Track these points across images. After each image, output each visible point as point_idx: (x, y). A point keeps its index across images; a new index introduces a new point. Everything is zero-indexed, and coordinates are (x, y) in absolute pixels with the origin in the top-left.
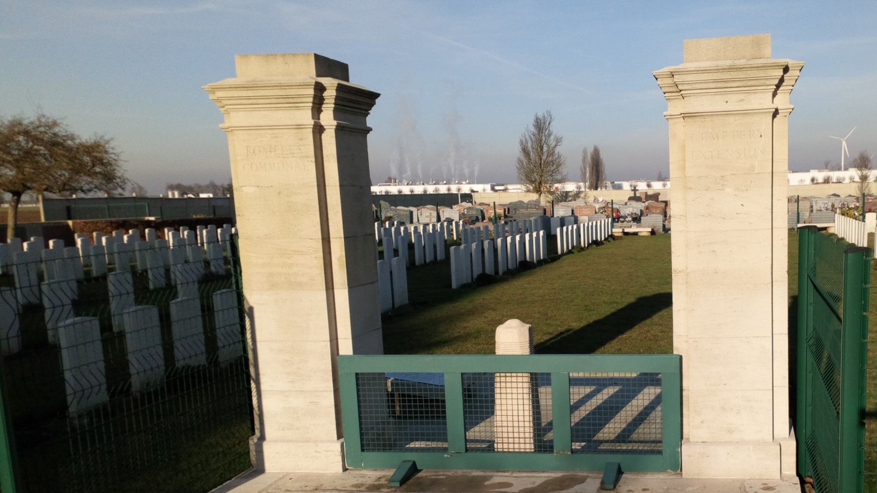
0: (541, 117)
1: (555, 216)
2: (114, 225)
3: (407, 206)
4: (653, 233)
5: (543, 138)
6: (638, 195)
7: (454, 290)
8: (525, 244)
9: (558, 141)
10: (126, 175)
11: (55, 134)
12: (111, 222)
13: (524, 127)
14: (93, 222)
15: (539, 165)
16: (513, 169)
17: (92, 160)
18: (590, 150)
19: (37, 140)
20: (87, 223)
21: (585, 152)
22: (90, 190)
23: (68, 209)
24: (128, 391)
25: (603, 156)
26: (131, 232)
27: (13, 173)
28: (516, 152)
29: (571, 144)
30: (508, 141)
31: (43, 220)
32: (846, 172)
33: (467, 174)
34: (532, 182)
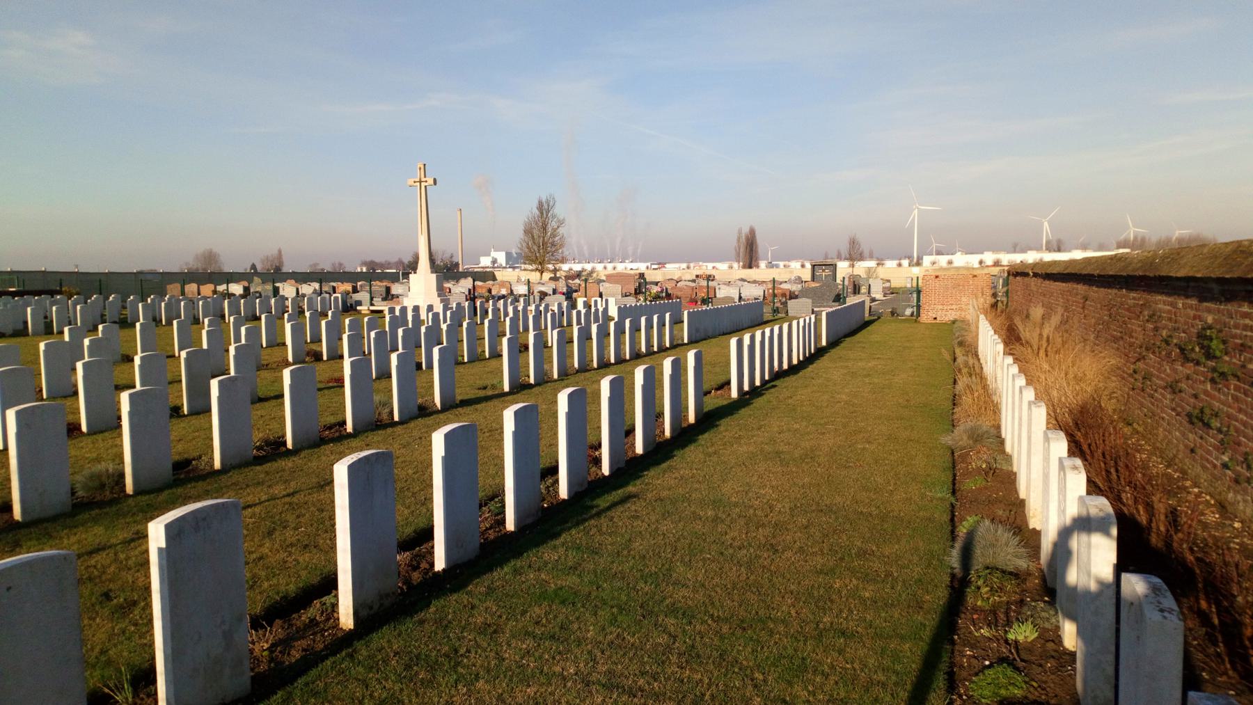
1: (925, 318)
8: (660, 415)
9: (561, 223)
13: (528, 210)
15: (540, 245)
18: (746, 230)
21: (740, 232)
30: (513, 223)
33: (630, 252)
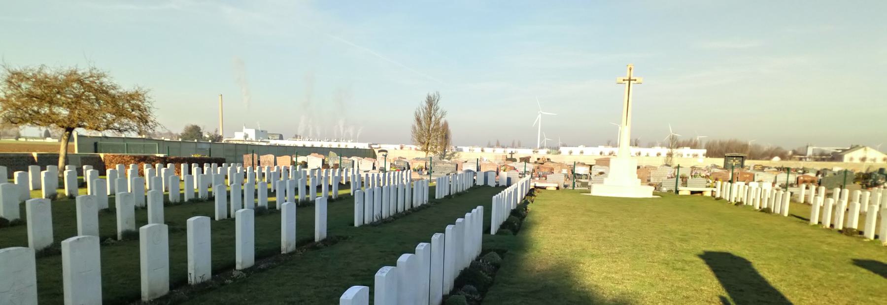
4: (558, 188)
9: (443, 114)
11: (101, 84)
12: (135, 157)
16: (409, 133)
17: (129, 107)
19: (89, 88)
22: (126, 130)
23: (96, 144)
26: (169, 165)
27: (67, 113)
28: (412, 121)
29: (453, 114)
31: (76, 152)
34: (423, 143)
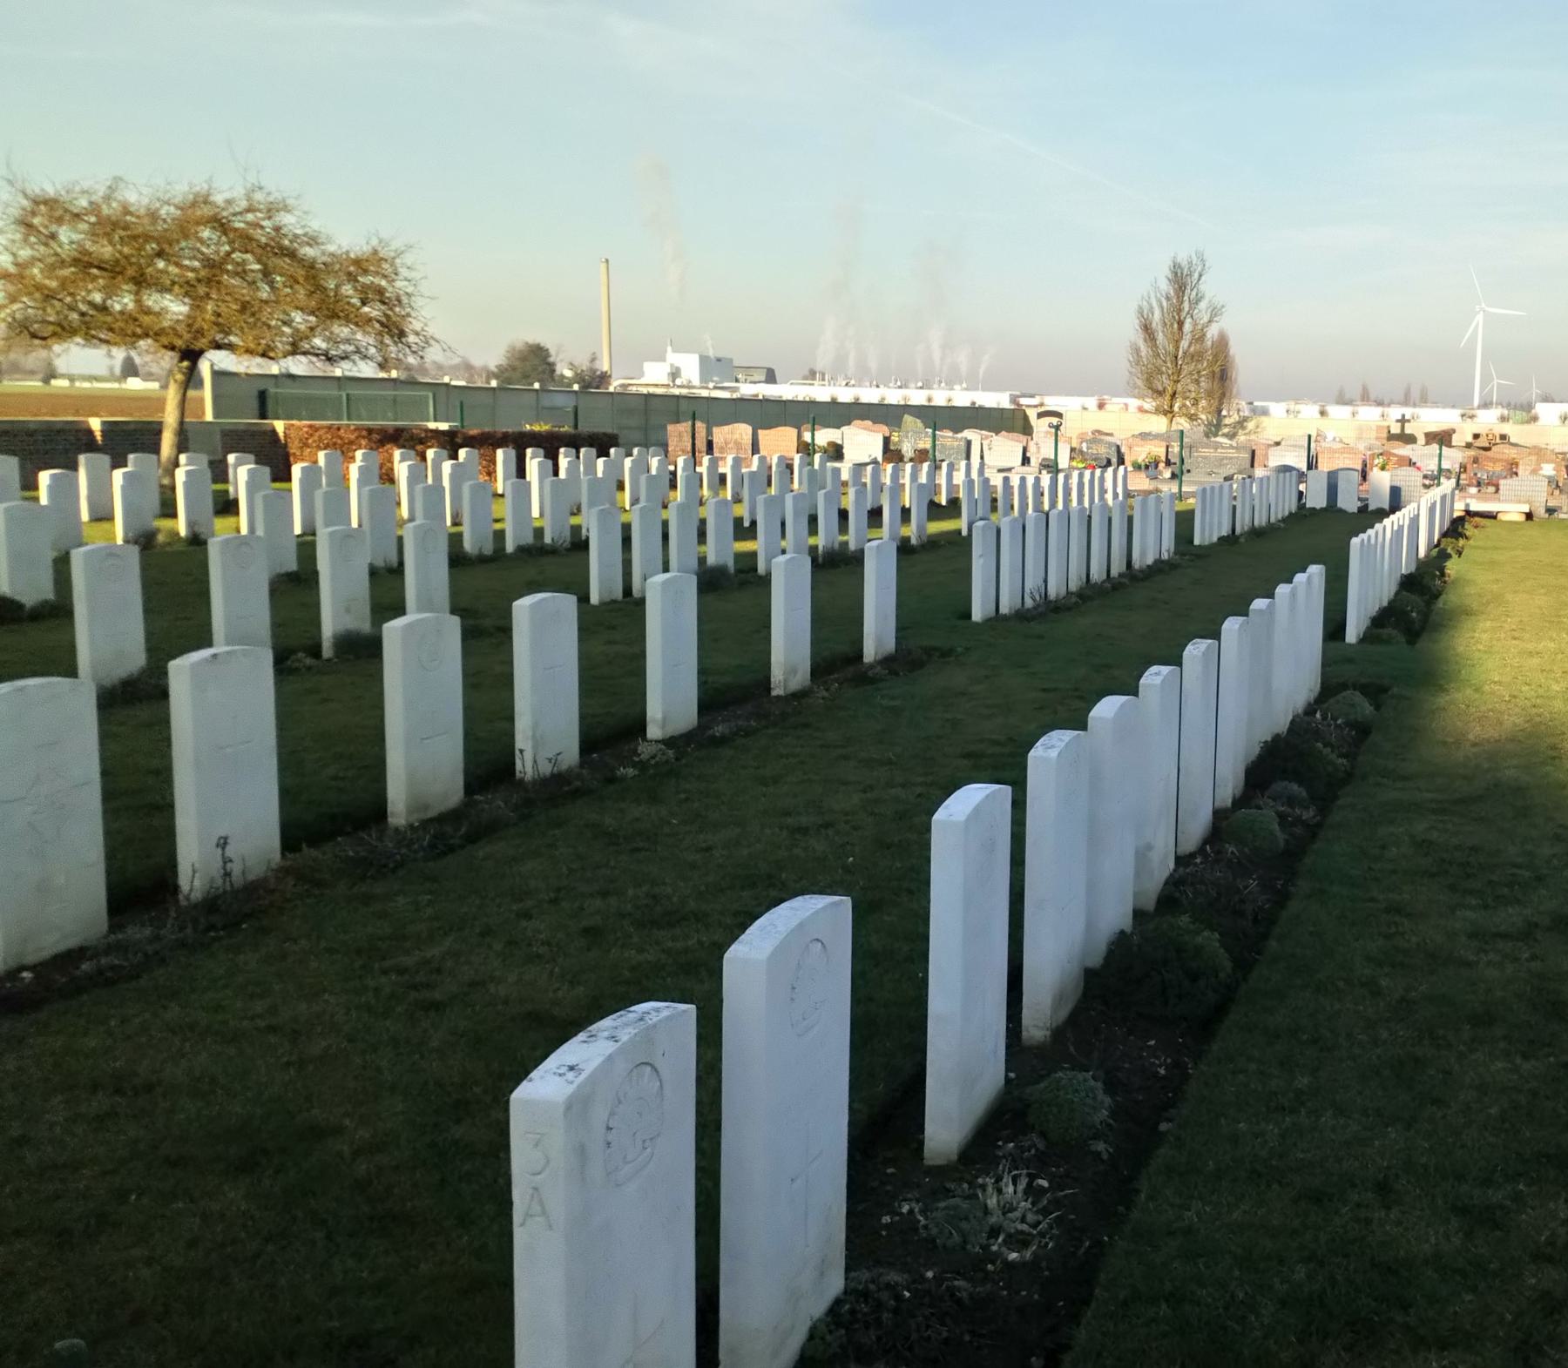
0: (1184, 264)
2: (375, 436)
3: (956, 431)
5: (1186, 306)
6: (1407, 431)
7: (977, 624)
9: (1215, 313)
10: (431, 330)
12: (370, 431)
14: (330, 428)
16: (1121, 364)
17: (355, 293)
19: (245, 241)
20: (314, 429)
22: (345, 357)
23: (262, 396)
24: (163, 881)
25: (1235, 349)
27: (184, 309)
28: (1130, 331)
32: (319, 533)
33: (964, 369)
34: (1160, 393)
